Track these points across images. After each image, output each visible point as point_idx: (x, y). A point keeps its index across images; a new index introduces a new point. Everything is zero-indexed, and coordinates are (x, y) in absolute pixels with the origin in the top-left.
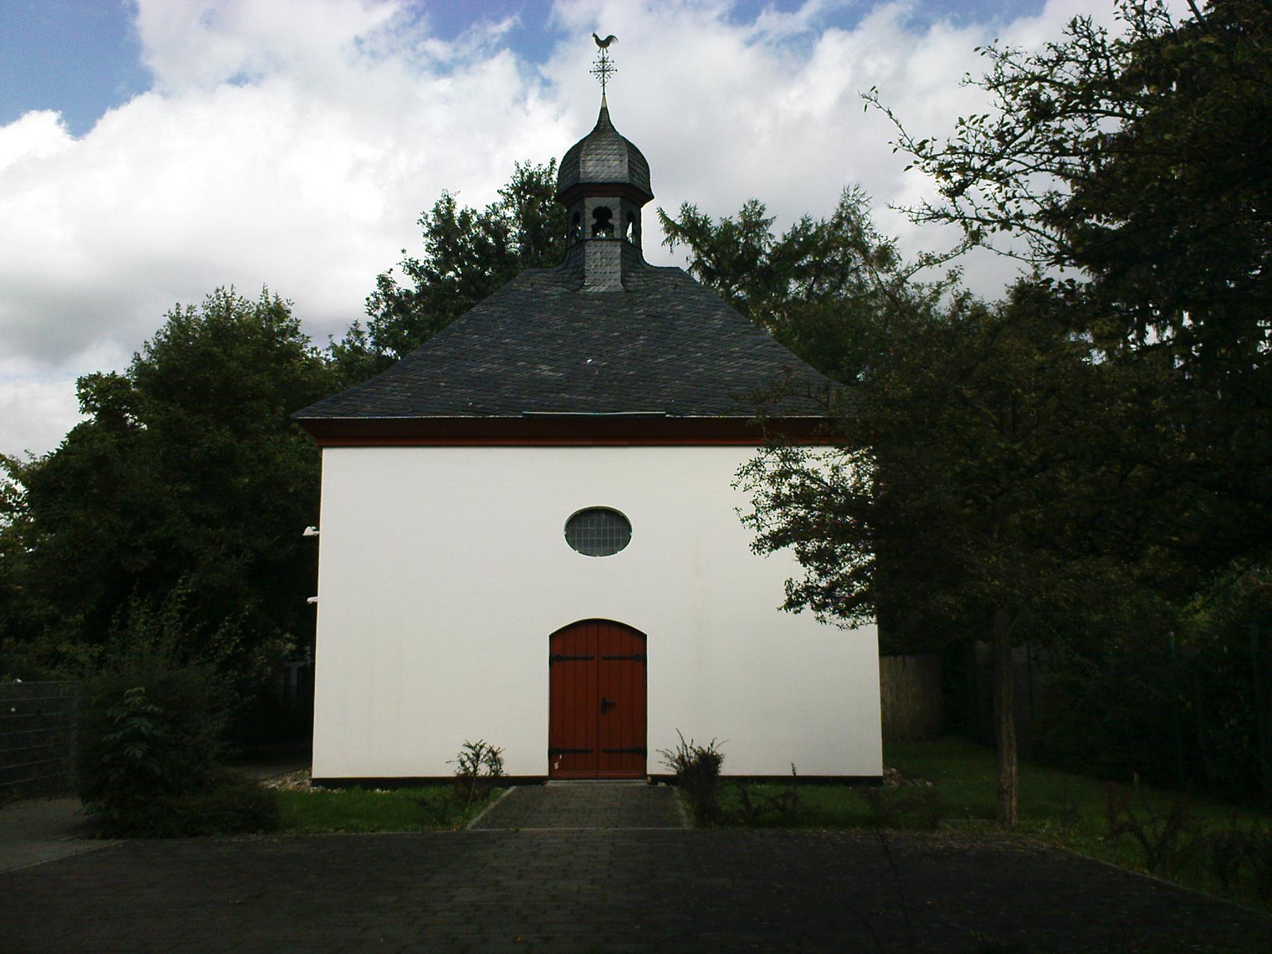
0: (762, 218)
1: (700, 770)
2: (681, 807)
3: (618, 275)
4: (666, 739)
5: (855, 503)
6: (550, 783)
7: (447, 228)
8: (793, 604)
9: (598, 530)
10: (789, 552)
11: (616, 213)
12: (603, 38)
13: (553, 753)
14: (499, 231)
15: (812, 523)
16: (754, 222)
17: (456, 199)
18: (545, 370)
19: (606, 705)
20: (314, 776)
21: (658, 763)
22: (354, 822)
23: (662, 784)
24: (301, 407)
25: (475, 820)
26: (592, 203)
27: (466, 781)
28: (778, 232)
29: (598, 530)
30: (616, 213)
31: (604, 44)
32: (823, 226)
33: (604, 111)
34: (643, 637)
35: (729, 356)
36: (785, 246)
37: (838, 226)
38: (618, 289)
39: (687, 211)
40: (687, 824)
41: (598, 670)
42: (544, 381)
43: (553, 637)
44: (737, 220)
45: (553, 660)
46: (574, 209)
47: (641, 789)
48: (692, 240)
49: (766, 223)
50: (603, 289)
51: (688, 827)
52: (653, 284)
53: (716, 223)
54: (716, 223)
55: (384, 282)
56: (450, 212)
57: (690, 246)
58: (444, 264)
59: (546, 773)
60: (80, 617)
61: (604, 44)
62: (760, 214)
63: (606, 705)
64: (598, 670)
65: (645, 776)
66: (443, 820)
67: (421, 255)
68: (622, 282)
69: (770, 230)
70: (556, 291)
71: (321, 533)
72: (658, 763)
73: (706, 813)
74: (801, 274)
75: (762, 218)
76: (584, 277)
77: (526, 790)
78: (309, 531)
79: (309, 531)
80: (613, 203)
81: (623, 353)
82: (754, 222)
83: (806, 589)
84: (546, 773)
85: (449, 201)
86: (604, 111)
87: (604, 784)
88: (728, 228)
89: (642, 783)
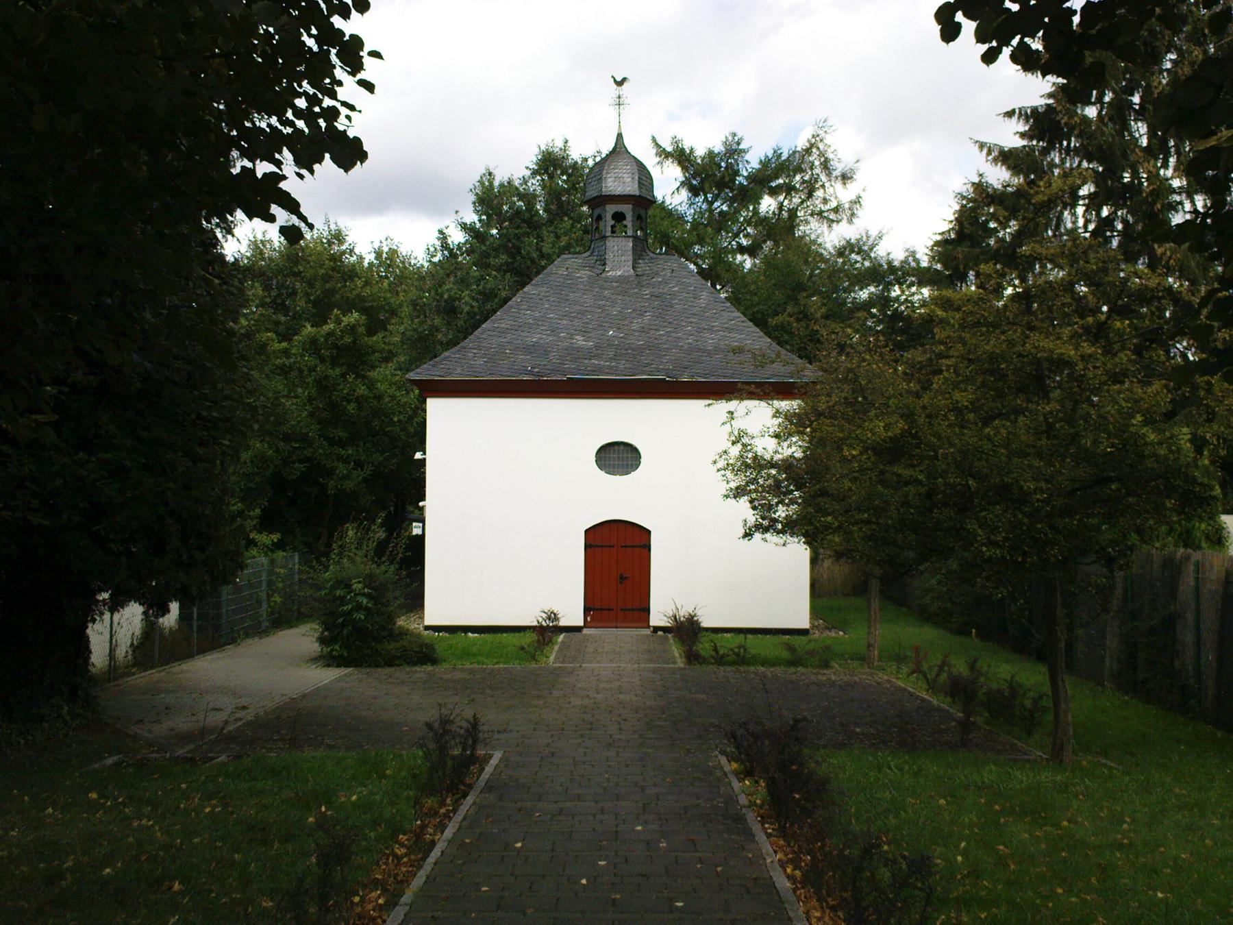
0: (741, 147)
1: (687, 630)
2: (676, 650)
3: (631, 263)
4: (664, 604)
5: (787, 466)
6: (585, 631)
7: (490, 198)
8: (748, 535)
9: (618, 457)
10: (744, 502)
11: (629, 216)
12: (619, 79)
13: (587, 610)
14: (529, 198)
15: (756, 480)
16: (734, 151)
17: (495, 172)
18: (580, 340)
19: (623, 579)
20: (427, 622)
21: (659, 616)
22: (480, 659)
23: (660, 633)
24: (771, 793)
25: (552, 657)
26: (611, 209)
27: (539, 630)
28: (752, 161)
29: (618, 457)
30: (629, 216)
31: (620, 83)
32: (794, 152)
33: (620, 136)
34: (649, 532)
35: (711, 330)
36: (759, 171)
37: (808, 151)
38: (630, 276)
39: (676, 142)
40: (680, 663)
41: (618, 555)
42: (579, 349)
43: (586, 531)
44: (719, 148)
45: (587, 547)
46: (597, 212)
47: (647, 636)
48: (680, 163)
49: (744, 151)
50: (619, 273)
51: (682, 665)
52: (655, 269)
53: (700, 152)
54: (700, 152)
55: (443, 236)
56: (491, 184)
57: (679, 169)
58: (487, 225)
59: (582, 624)
60: (258, 511)
61: (620, 83)
62: (738, 144)
63: (623, 579)
64: (618, 555)
65: (649, 626)
66: (534, 658)
67: (471, 217)
68: (634, 267)
69: (747, 157)
70: (585, 274)
71: (428, 457)
72: (659, 616)
73: (692, 657)
74: (774, 192)
75: (741, 147)
76: (605, 264)
77: (572, 635)
78: (418, 456)
79: (418, 456)
80: (627, 209)
81: (635, 326)
82: (734, 151)
83: (756, 526)
84: (582, 624)
85: (490, 174)
86: (620, 136)
87: (628, 632)
88: (711, 154)
89: (648, 632)
